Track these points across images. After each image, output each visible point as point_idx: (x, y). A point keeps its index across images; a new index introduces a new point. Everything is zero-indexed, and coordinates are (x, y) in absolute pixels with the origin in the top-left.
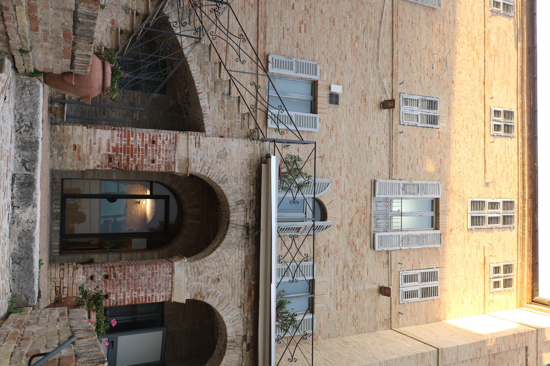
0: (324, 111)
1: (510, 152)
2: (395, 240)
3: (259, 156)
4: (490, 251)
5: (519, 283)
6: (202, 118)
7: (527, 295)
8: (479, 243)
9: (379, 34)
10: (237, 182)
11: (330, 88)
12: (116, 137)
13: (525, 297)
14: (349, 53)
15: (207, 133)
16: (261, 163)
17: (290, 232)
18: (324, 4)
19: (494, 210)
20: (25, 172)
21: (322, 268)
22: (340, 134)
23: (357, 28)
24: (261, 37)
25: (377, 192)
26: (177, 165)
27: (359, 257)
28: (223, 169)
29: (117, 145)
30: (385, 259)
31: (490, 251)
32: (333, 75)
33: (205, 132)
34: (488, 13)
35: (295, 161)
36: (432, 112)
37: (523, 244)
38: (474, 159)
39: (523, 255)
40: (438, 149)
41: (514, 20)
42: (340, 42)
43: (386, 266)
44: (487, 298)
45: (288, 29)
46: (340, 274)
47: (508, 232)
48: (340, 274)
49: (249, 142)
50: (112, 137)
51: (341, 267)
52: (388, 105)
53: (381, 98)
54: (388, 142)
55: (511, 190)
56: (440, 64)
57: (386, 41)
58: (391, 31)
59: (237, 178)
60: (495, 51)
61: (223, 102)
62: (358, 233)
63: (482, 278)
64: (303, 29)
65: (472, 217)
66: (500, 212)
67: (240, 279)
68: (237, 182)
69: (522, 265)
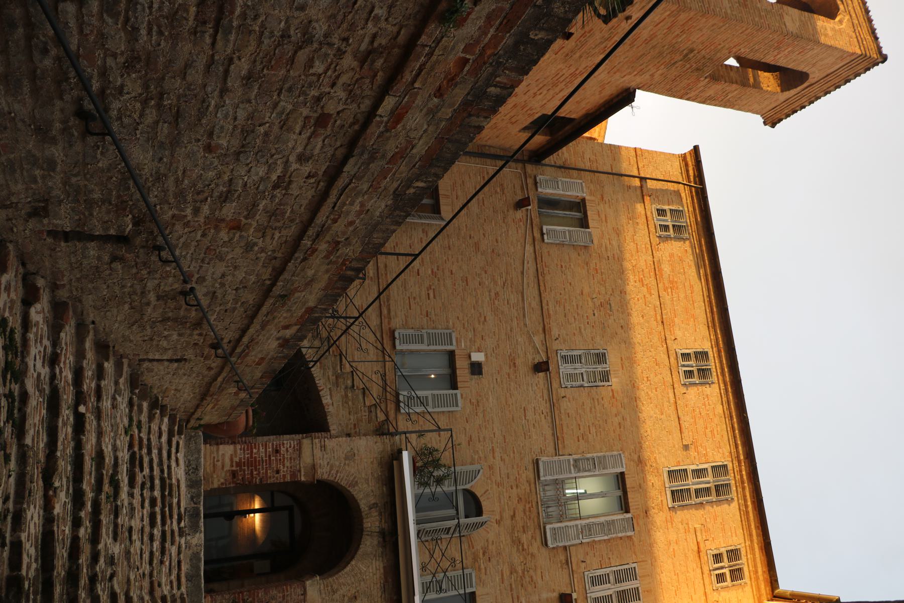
2: (573, 532)
6: (326, 416)
7: (764, 589)
8: (688, 524)
9: (523, 286)
10: (368, 484)
11: (470, 357)
12: (239, 451)
13: (763, 591)
15: (332, 432)
20: (193, 505)
21: (483, 577)
23: (496, 283)
24: (385, 311)
25: (542, 474)
26: (303, 473)
27: (529, 558)
29: (240, 459)
30: (563, 558)
33: (329, 431)
34: (655, 240)
35: (430, 453)
36: (600, 368)
38: (663, 417)
39: (751, 535)
40: (614, 411)
41: (691, 242)
42: (477, 302)
43: (565, 566)
44: (709, 597)
45: (414, 298)
48: (506, 582)
49: (378, 438)
50: (235, 451)
51: (507, 573)
52: (541, 367)
56: (602, 309)
57: (531, 293)
58: (536, 280)
60: (671, 282)
61: (346, 396)
62: (523, 527)
64: (431, 295)
65: (673, 492)
66: (709, 480)
67: (380, 595)
68: (368, 484)
69: (752, 549)
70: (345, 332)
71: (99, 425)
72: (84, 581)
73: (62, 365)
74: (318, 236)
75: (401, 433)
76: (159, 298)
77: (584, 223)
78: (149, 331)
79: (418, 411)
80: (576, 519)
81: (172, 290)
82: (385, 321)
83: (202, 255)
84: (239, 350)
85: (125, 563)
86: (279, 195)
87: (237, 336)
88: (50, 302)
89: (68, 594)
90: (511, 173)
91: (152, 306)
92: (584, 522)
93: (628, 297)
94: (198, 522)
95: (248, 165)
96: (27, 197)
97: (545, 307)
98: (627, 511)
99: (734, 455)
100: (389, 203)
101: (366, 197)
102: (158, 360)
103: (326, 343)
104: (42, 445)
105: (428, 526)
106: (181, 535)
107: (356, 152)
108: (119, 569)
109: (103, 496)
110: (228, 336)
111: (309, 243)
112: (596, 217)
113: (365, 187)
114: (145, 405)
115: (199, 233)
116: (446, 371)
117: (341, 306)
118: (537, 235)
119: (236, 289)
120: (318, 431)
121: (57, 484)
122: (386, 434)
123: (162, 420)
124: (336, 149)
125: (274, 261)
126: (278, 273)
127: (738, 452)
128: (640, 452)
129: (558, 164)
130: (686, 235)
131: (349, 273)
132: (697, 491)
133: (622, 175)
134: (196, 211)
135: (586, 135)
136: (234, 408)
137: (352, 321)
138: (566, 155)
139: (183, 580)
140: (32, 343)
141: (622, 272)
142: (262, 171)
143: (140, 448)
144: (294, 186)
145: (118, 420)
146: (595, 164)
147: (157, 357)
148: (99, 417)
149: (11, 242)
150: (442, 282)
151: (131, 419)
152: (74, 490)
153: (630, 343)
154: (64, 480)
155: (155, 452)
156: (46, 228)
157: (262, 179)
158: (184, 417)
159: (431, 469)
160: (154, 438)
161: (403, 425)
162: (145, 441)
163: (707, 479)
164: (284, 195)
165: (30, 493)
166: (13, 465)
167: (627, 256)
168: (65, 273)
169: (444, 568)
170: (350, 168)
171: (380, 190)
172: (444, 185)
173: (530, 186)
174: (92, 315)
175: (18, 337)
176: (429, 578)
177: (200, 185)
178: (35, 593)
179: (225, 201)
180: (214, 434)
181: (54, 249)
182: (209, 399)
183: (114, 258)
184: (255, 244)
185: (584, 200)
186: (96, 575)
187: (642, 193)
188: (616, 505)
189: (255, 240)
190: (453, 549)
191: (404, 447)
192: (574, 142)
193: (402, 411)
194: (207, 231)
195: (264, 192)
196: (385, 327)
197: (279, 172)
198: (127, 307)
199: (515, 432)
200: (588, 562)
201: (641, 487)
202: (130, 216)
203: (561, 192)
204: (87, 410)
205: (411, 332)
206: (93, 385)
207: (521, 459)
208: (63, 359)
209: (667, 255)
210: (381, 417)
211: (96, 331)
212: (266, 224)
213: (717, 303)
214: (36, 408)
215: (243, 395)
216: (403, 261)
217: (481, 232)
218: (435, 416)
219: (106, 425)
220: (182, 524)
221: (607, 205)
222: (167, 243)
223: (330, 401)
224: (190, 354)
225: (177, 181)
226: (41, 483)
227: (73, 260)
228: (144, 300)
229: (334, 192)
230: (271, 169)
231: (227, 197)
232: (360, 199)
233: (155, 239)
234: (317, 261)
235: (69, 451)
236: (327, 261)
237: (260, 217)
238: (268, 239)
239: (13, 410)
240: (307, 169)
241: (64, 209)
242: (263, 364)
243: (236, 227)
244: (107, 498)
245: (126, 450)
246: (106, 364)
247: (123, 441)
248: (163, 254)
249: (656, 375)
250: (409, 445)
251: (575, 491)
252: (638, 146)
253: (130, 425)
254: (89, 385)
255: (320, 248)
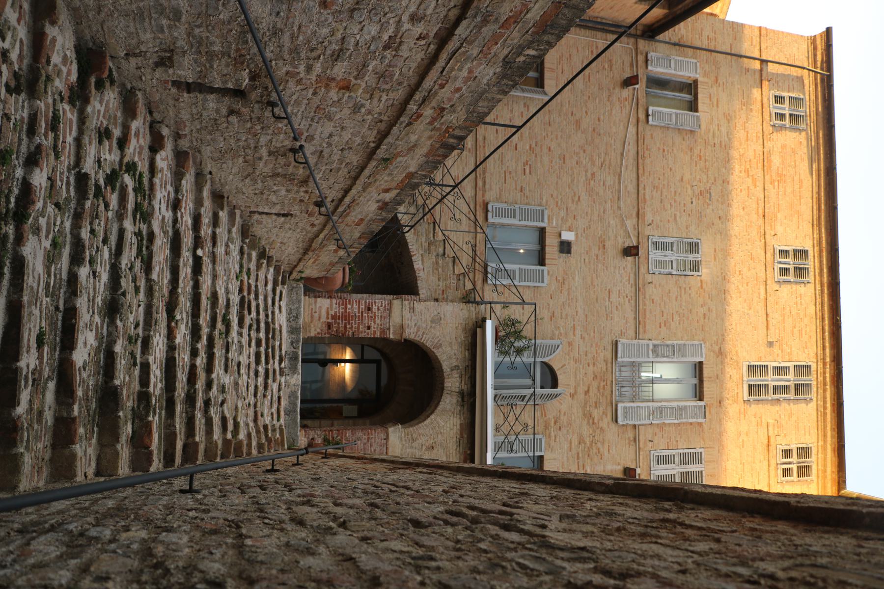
0: (554, 262)
1: (803, 302)
2: (643, 413)
3: (474, 320)
4: (776, 429)
5: (820, 472)
6: (416, 280)
8: (761, 418)
12: (334, 306)
14: (583, 194)
15: (421, 296)
16: (477, 327)
17: (504, 401)
18: (552, 140)
19: (781, 377)
21: (552, 443)
22: (573, 288)
23: (593, 163)
24: (480, 184)
25: (619, 355)
26: (391, 331)
27: (598, 431)
28: (438, 334)
30: (631, 435)
31: (776, 429)
32: (565, 220)
34: (768, 129)
35: (513, 324)
36: (692, 257)
37: (825, 421)
38: (751, 312)
39: (825, 436)
41: (807, 134)
42: (572, 181)
43: (632, 443)
45: (510, 173)
46: (574, 451)
47: (802, 406)
48: (574, 451)
50: (331, 305)
51: (575, 442)
52: (631, 251)
53: (624, 243)
54: (633, 295)
55: (806, 351)
56: (701, 197)
57: (629, 176)
58: (635, 163)
59: (451, 343)
61: (437, 263)
62: (596, 403)
63: (766, 463)
64: (527, 171)
65: (750, 386)
66: (790, 379)
69: (824, 449)
70: (440, 201)
71: (214, 269)
72: (199, 403)
73: (183, 210)
74: (424, 101)
75: (486, 303)
76: (270, 153)
77: (693, 106)
78: (260, 185)
79: (504, 283)
80: (648, 401)
81: (283, 146)
82: (480, 193)
83: (312, 114)
84: (340, 209)
85: (234, 393)
86: (389, 56)
87: (340, 196)
88: (173, 150)
89: (187, 413)
90: (623, 48)
91: (263, 161)
92: (655, 405)
93: (730, 187)
94: (296, 365)
95: (360, 23)
96: (154, 47)
97: (641, 192)
98: (701, 399)
99: (820, 356)
100: (498, 70)
101: (475, 63)
102: (267, 214)
103: (421, 210)
104: (166, 281)
105: (505, 392)
106: (281, 374)
107: (470, 13)
108: (229, 397)
109: (217, 332)
110: (332, 195)
111: (415, 108)
112: (707, 101)
113: (475, 52)
114: (254, 254)
115: (311, 91)
116: (536, 247)
117: (438, 176)
118: (642, 116)
119: (342, 150)
120: (408, 294)
121: (178, 317)
122: (472, 303)
123: (268, 270)
124: (449, 10)
125: (379, 124)
126: (383, 136)
127: (824, 354)
128: (722, 343)
129: (672, 41)
130: (803, 126)
131: (452, 141)
132: (776, 388)
133: (741, 56)
134: (309, 68)
135: (707, 10)
136: (332, 265)
137: (448, 189)
138: (683, 31)
139: (282, 413)
140: (158, 187)
141: (728, 160)
142: (374, 30)
143: (249, 294)
144: (404, 47)
145: (231, 264)
146: (713, 43)
147: (266, 211)
148: (214, 262)
149: (140, 90)
150: (539, 158)
151: (241, 266)
152: (192, 324)
153: (726, 235)
154: (184, 314)
155: (261, 298)
156: (171, 78)
157: (374, 39)
158: (287, 269)
159: (512, 340)
160: (261, 285)
161: (489, 295)
162: (253, 288)
163: (788, 377)
164: (394, 57)
165: (156, 322)
166: (142, 296)
167: (736, 144)
168: (187, 124)
169: (517, 431)
170: (462, 31)
171: (490, 56)
172: (550, 59)
173: (640, 63)
174: (209, 166)
175: (145, 180)
176: (501, 439)
177: (314, 42)
178: (161, 409)
179: (336, 60)
180: (314, 287)
181: (177, 100)
182: (310, 253)
183: (231, 112)
184: (363, 106)
185: (696, 82)
186: (209, 399)
187: (761, 77)
188: (691, 392)
189: (363, 102)
190: (526, 415)
191: (488, 316)
192: (693, 17)
193: (489, 282)
194: (318, 90)
195: (375, 52)
196: (480, 199)
197: (391, 31)
198: (241, 160)
199: (598, 312)
200: (656, 441)
201: (719, 378)
202: (247, 70)
203: (673, 72)
204: (204, 253)
205: (504, 206)
206: (210, 231)
207: (601, 339)
208: (184, 205)
209: (779, 146)
210: (469, 286)
211: (212, 181)
212: (374, 85)
213: (826, 201)
214: (161, 247)
215: (342, 253)
216: (506, 133)
217: (584, 109)
218: (521, 290)
219: (220, 269)
220: (283, 365)
221: (721, 88)
222: (280, 99)
223: (422, 267)
224: (296, 210)
225: (293, 38)
226: (165, 314)
227: (195, 111)
228: (257, 155)
229: (444, 56)
230: (383, 27)
231: (338, 55)
232: (469, 65)
233: (269, 95)
234: (422, 127)
235: (189, 289)
236: (431, 127)
237: (369, 78)
238: (375, 100)
239: (141, 248)
240: (419, 29)
241: (187, 61)
242: (362, 225)
243: (346, 87)
244: (220, 334)
245: (237, 294)
246: (221, 213)
247: (234, 285)
248: (276, 110)
249: (749, 270)
250: (493, 314)
251: (650, 375)
252: (763, 25)
253: (241, 272)
254: (206, 231)
255: (425, 113)
